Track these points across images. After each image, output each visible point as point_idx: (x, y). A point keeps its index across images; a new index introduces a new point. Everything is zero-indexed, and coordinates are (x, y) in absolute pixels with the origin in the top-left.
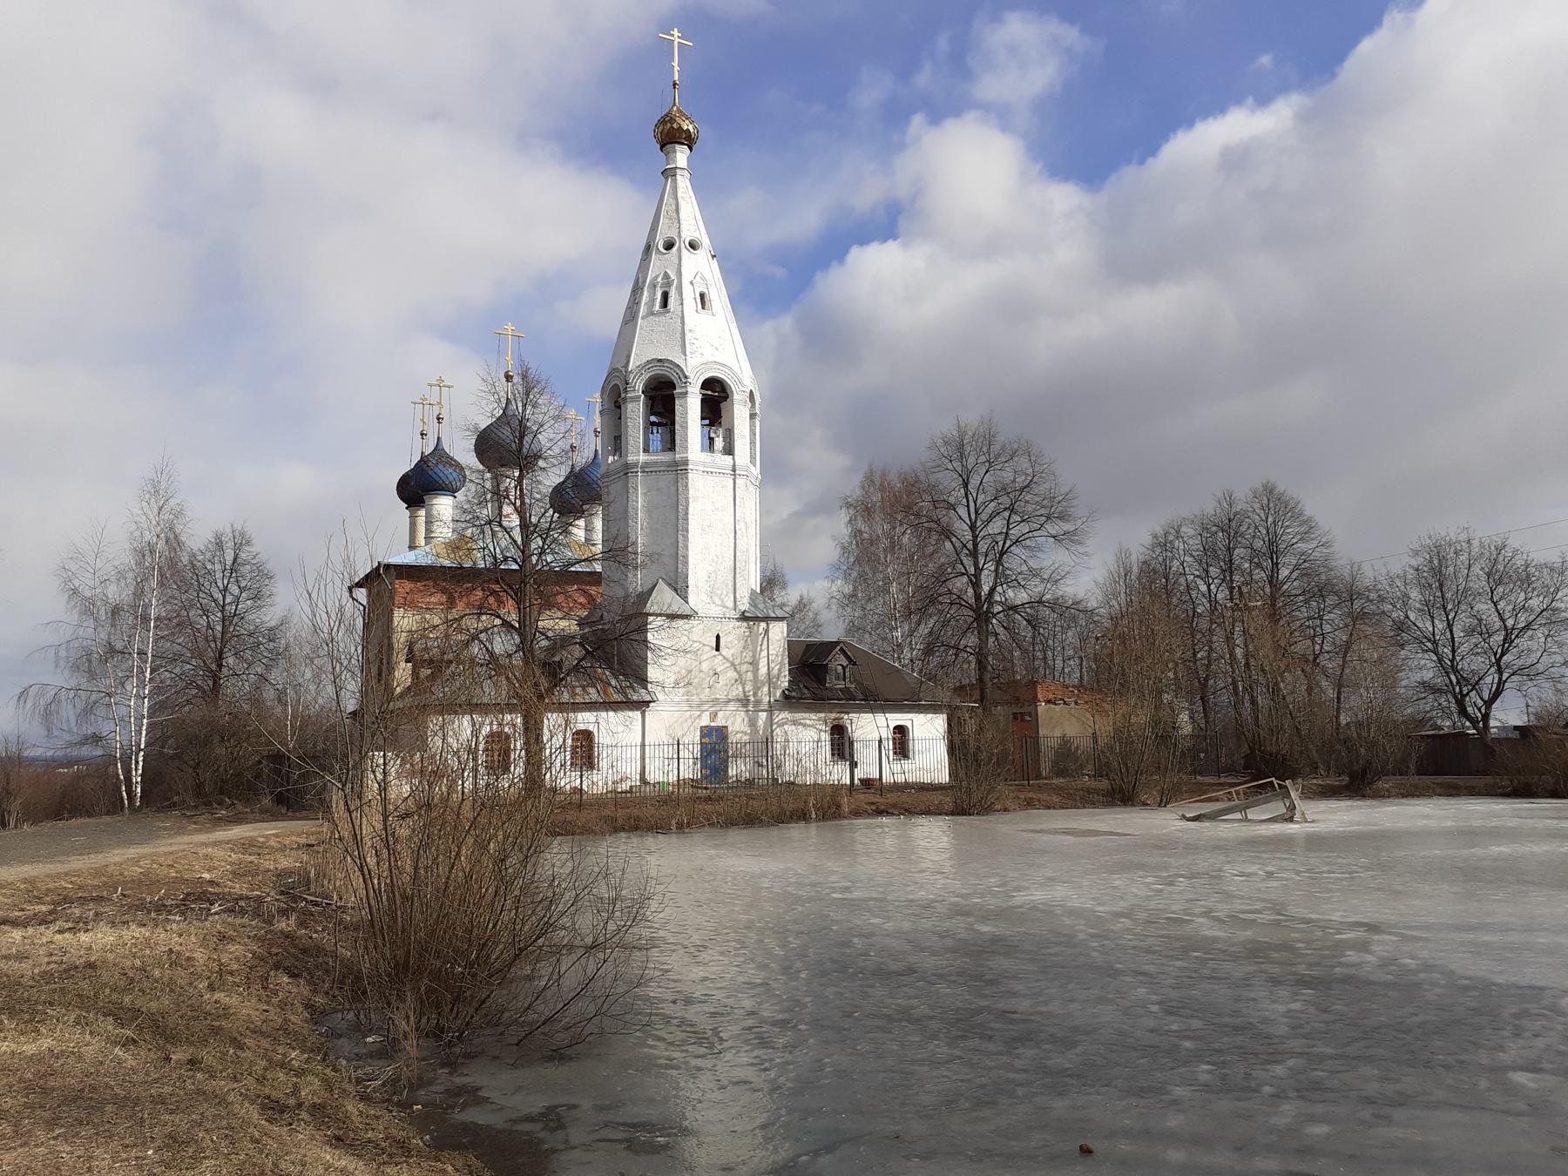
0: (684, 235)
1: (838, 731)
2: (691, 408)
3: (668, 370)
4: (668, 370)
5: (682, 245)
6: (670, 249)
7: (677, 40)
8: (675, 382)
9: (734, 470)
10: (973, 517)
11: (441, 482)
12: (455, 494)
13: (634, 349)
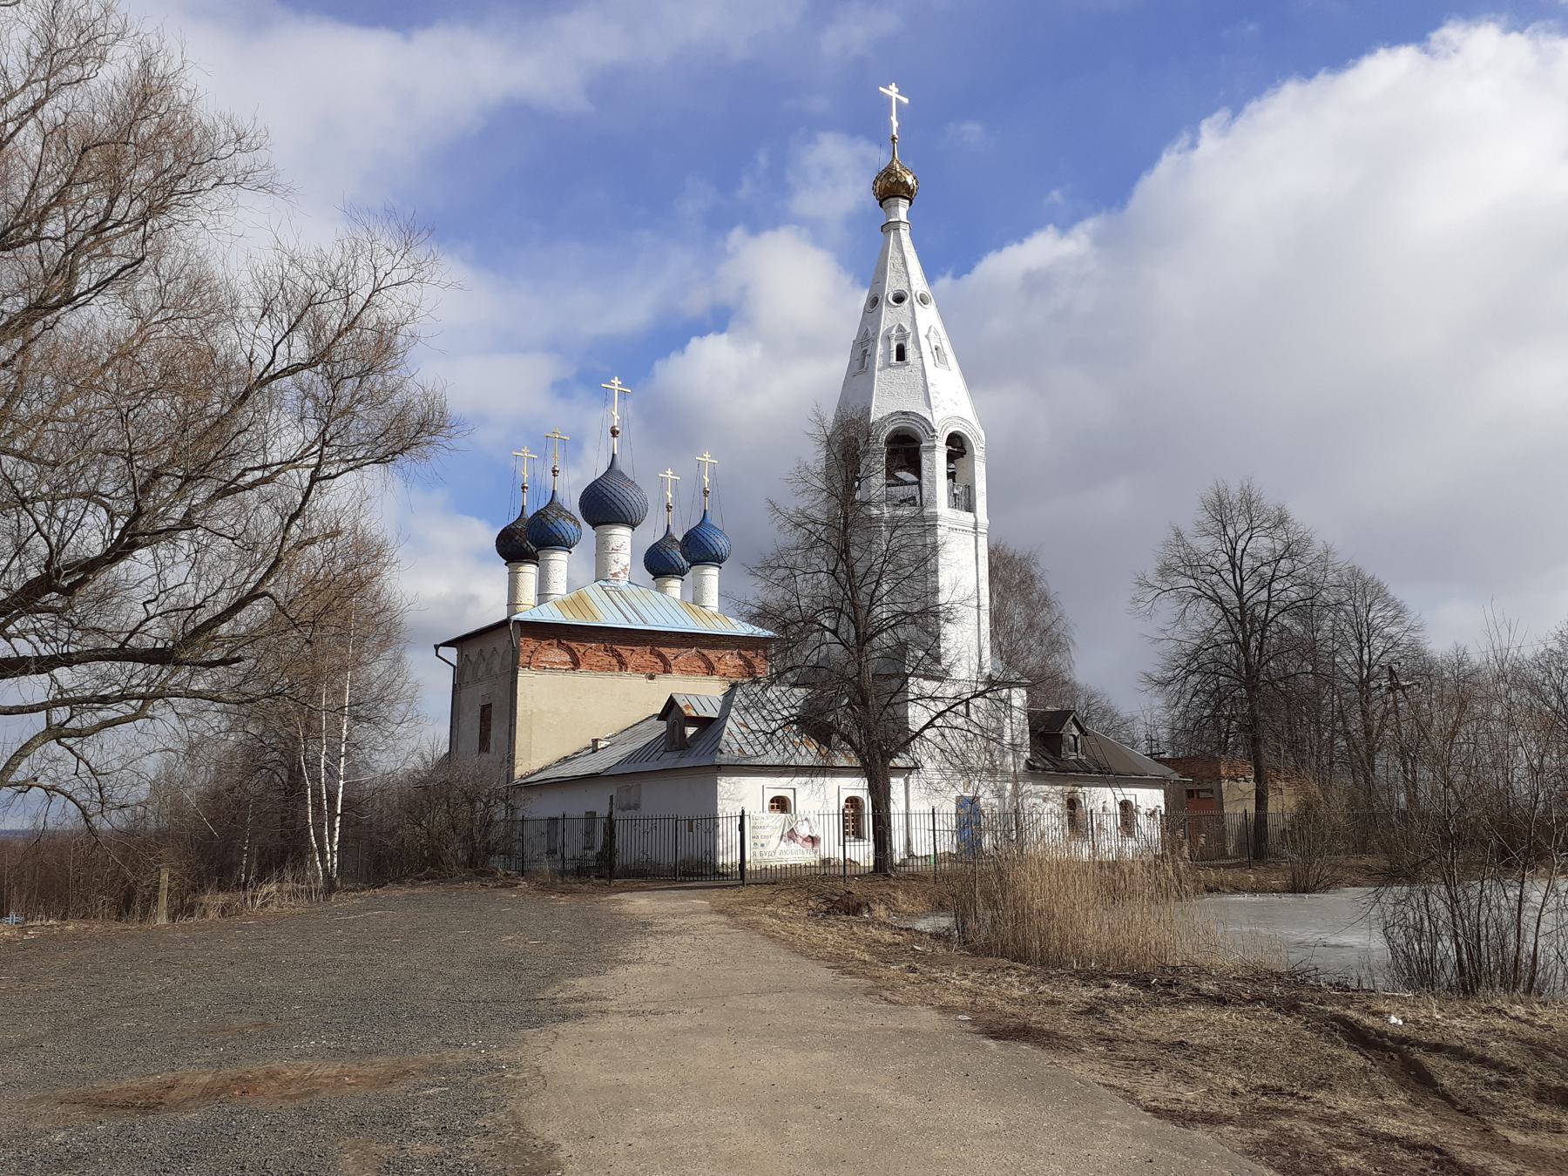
0: (914, 288)
1: (1072, 804)
2: (937, 461)
3: (918, 425)
4: (918, 425)
5: (914, 298)
6: (901, 302)
8: (922, 435)
9: (976, 529)
11: (560, 537)
12: (571, 550)
13: (874, 400)
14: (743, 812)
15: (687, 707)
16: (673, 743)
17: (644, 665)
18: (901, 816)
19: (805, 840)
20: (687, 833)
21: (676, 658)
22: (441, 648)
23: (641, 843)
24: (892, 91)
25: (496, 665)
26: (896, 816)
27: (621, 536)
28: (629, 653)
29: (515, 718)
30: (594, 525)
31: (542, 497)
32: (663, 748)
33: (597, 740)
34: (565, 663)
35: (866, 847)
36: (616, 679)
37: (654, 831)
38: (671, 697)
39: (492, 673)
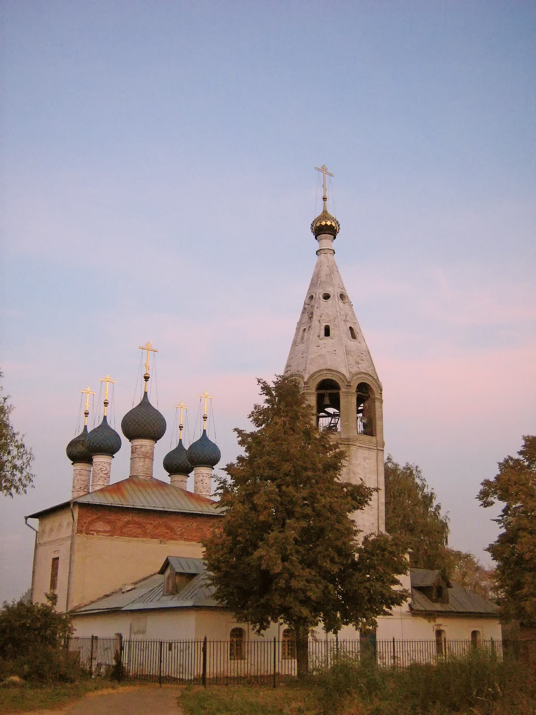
14: (206, 639)
20: (168, 652)
22: (29, 519)
23: (219, 658)
30: (131, 437)
31: (97, 420)
32: (162, 593)
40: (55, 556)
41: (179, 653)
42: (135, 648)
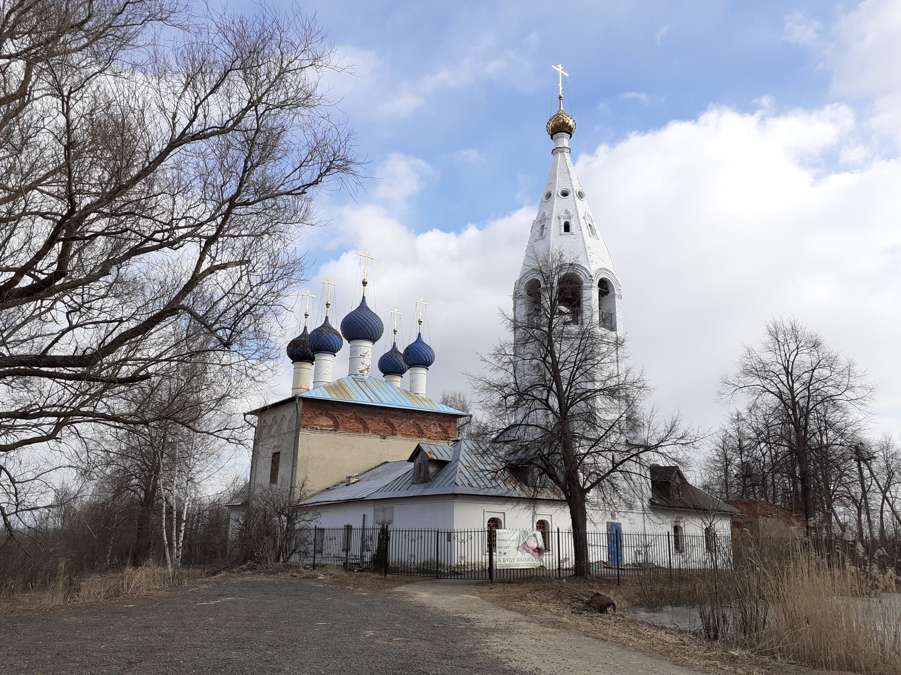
2: (592, 296)
7: (561, 71)
10: (791, 384)
15: (429, 452)
16: (419, 478)
17: (380, 429)
18: (604, 535)
19: (534, 550)
20: (446, 542)
21: (400, 426)
24: (559, 69)
25: (285, 428)
26: (590, 535)
27: (366, 346)
28: (370, 421)
29: (297, 461)
30: (350, 339)
32: (411, 481)
33: (350, 477)
34: (330, 426)
35: (551, 556)
36: (362, 438)
37: (420, 540)
38: (418, 445)
39: (281, 432)
40: (277, 450)
41: (410, 542)
42: (404, 539)
